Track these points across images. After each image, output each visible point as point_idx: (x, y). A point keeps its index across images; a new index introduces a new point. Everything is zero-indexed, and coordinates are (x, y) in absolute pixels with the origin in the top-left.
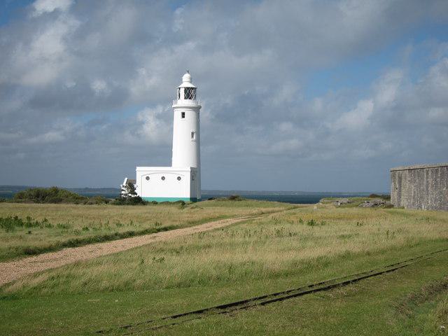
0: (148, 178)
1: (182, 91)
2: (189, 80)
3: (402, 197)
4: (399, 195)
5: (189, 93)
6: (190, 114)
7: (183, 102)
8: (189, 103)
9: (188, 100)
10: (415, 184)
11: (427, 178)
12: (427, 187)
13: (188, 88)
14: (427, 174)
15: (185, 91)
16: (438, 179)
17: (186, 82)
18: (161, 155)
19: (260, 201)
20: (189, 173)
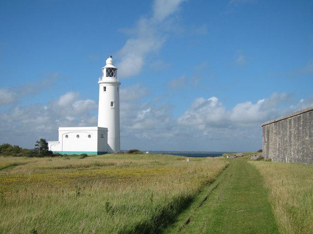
0: (67, 136)
1: (105, 71)
2: (110, 62)
3: (270, 149)
4: (268, 148)
5: (111, 72)
6: (110, 88)
7: (106, 79)
8: (110, 79)
9: (109, 78)
10: (280, 136)
11: (290, 129)
12: (290, 138)
13: (109, 68)
14: (290, 123)
15: (107, 71)
16: (301, 128)
17: (109, 63)
18: (88, 117)
19: (203, 158)
20: (97, 132)
